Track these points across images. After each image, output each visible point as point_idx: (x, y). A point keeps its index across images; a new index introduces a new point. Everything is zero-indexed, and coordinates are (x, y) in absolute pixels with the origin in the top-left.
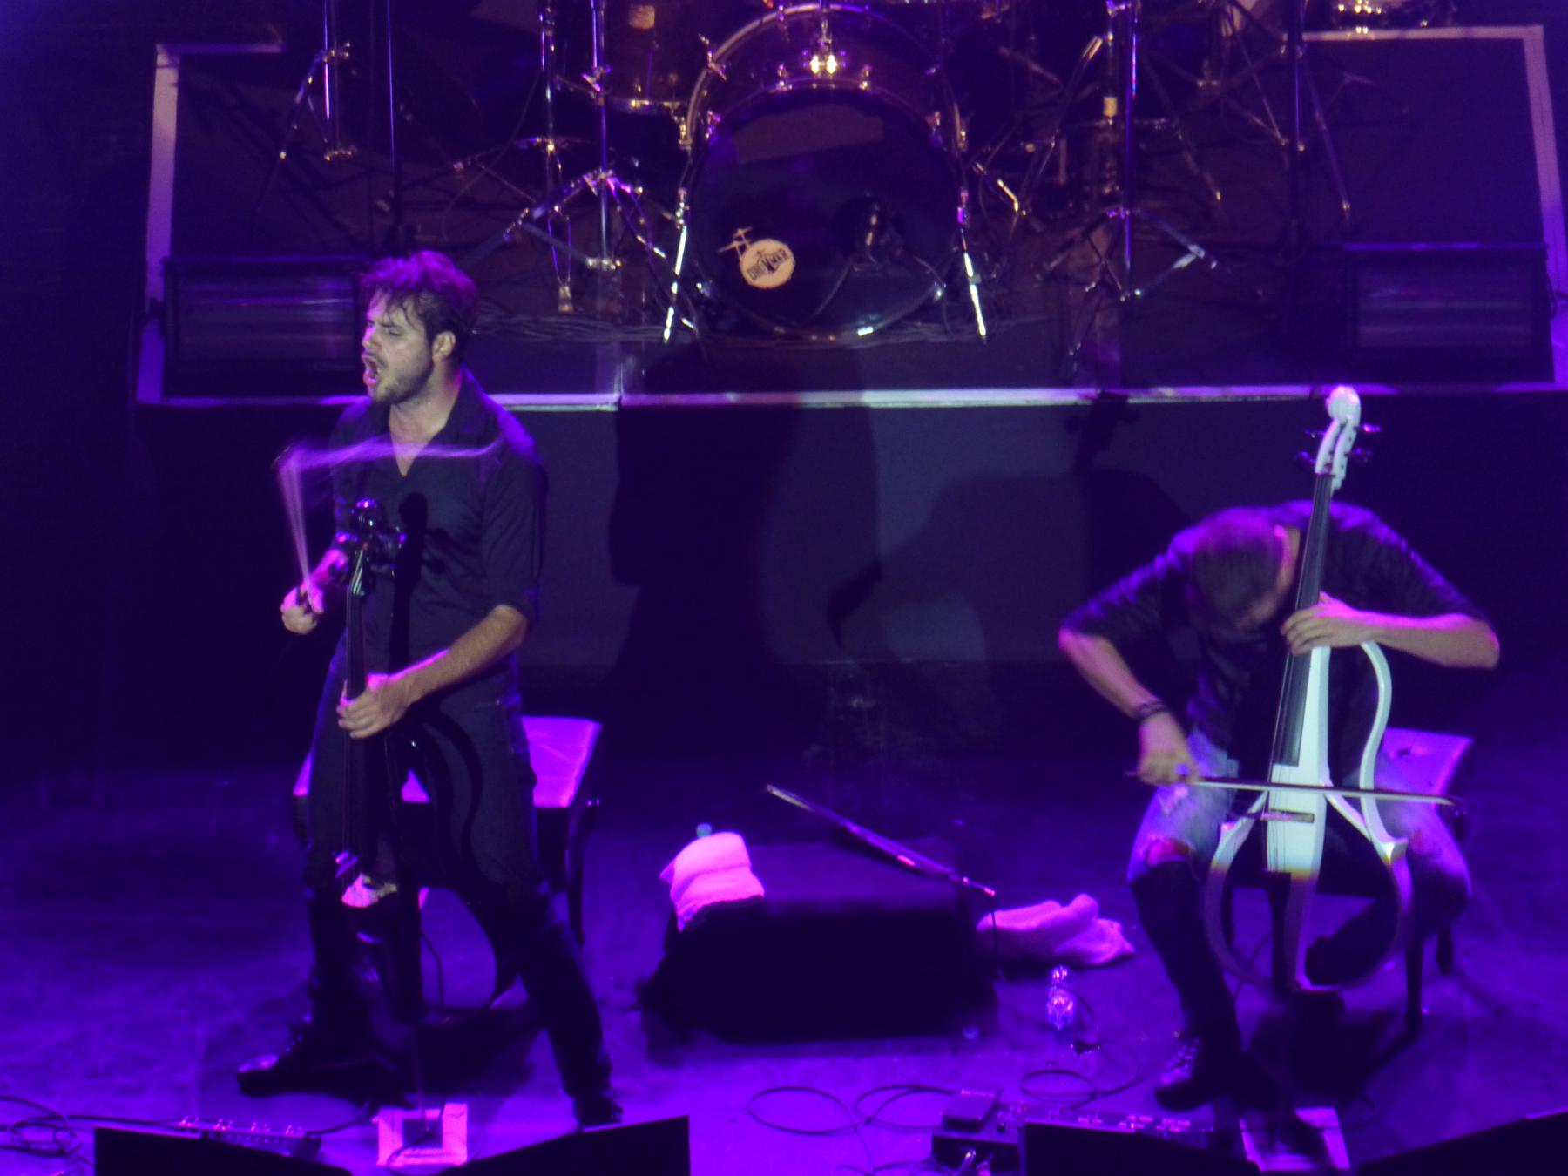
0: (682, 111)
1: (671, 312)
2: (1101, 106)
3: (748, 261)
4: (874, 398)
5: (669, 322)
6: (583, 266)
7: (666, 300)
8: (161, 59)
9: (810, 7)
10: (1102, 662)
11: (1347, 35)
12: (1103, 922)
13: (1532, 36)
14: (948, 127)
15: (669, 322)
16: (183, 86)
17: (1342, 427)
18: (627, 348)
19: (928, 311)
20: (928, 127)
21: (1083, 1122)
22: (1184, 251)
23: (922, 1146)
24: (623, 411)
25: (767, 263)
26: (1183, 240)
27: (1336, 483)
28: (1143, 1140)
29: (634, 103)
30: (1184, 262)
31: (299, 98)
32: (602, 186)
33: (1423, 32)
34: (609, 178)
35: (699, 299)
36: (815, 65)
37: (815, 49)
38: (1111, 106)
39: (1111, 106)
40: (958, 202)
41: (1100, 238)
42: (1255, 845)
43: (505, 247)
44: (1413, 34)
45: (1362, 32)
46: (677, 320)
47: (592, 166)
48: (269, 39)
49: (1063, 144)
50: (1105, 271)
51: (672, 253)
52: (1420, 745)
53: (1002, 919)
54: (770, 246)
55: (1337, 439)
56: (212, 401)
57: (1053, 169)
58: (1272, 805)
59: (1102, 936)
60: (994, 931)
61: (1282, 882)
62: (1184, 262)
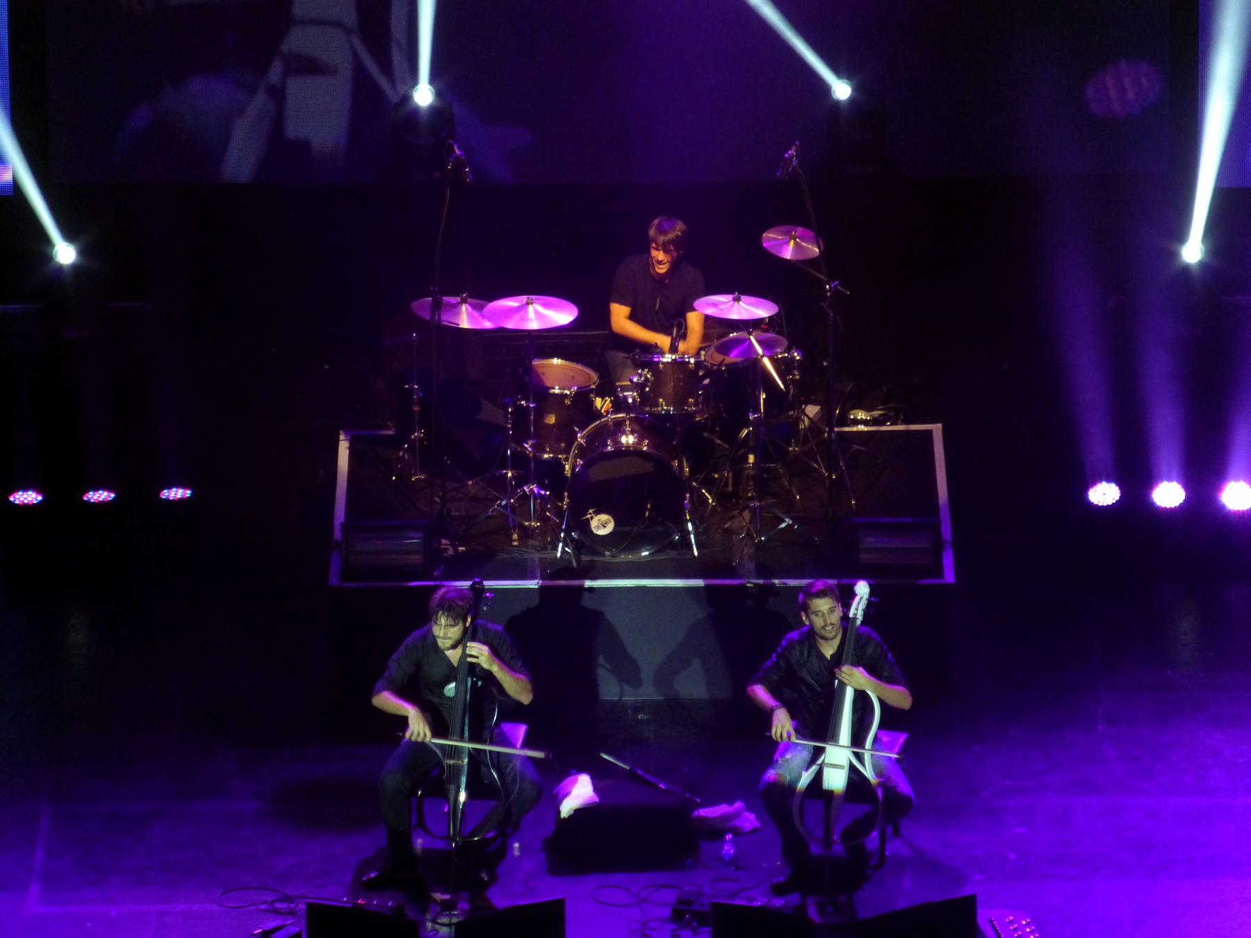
0: (566, 459)
3: (594, 524)
8: (342, 437)
10: (761, 693)
11: (855, 429)
12: (747, 814)
13: (937, 429)
14: (681, 467)
16: (351, 449)
19: (673, 546)
21: (738, 902)
22: (783, 521)
23: (667, 912)
24: (542, 589)
25: (602, 525)
26: (782, 516)
27: (858, 622)
28: (762, 909)
29: (546, 456)
30: (783, 525)
32: (531, 491)
34: (534, 487)
35: (573, 540)
36: (624, 439)
37: (624, 433)
38: (751, 458)
39: (751, 458)
40: (685, 498)
41: (747, 515)
42: (819, 777)
43: (490, 517)
44: (884, 428)
45: (861, 428)
47: (527, 483)
48: (389, 428)
50: (748, 530)
53: (703, 812)
54: (604, 517)
56: (386, 584)
57: (726, 485)
60: (699, 818)
61: (830, 793)
62: (783, 525)
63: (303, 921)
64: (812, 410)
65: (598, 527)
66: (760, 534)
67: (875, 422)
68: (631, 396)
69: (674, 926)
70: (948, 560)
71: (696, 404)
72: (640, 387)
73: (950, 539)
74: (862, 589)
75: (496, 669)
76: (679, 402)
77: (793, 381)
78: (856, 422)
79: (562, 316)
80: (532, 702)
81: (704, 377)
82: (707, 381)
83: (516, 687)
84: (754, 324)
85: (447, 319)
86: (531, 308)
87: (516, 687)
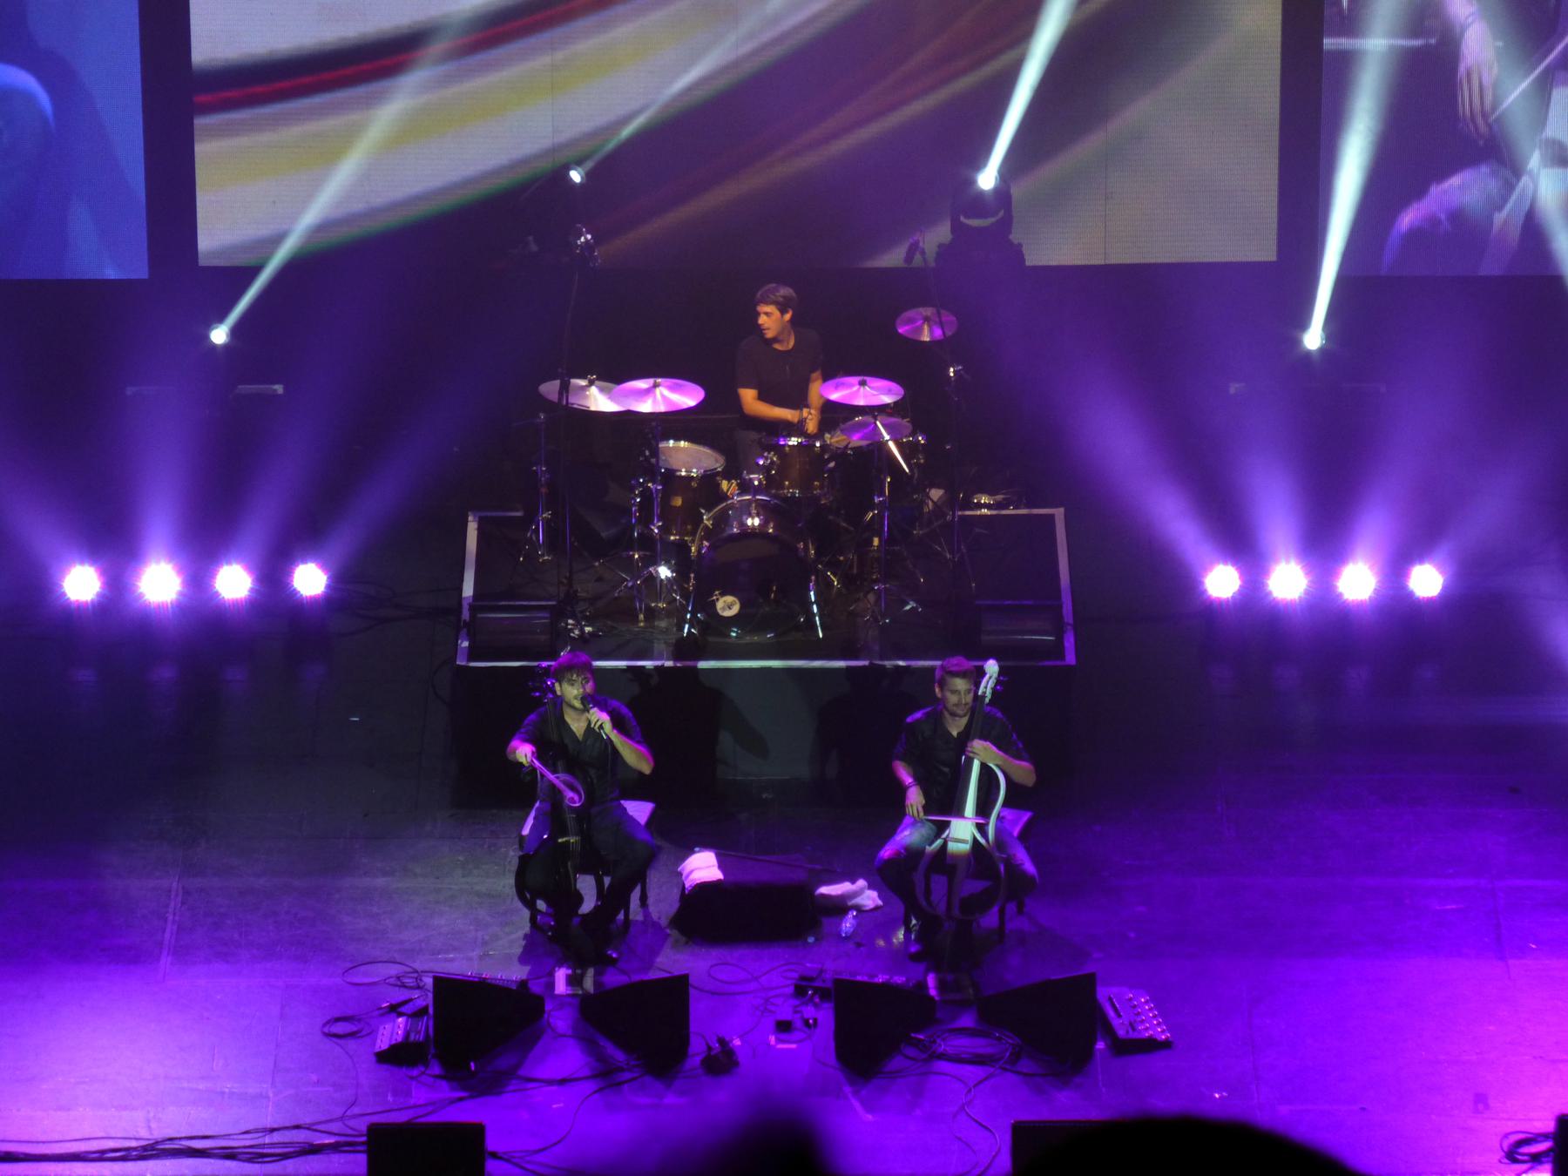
3: (720, 605)
4: (841, 664)
13: (1059, 513)
14: (806, 549)
16: (480, 529)
21: (859, 978)
23: (790, 990)
25: (727, 606)
28: (886, 987)
33: (1011, 511)
35: (699, 621)
38: (876, 541)
39: (876, 541)
41: (871, 597)
44: (1004, 512)
45: (984, 511)
53: (824, 890)
54: (730, 599)
57: (851, 567)
60: (823, 895)
63: (430, 995)
64: (936, 494)
66: (884, 616)
67: (998, 506)
68: (756, 479)
69: (797, 1002)
70: (1069, 642)
71: (821, 487)
72: (766, 470)
74: (992, 667)
75: (615, 738)
76: (805, 485)
77: (917, 464)
78: (980, 506)
79: (686, 398)
81: (829, 461)
82: (832, 465)
83: (634, 757)
84: (882, 409)
85: (576, 401)
86: (658, 391)
87: (634, 757)
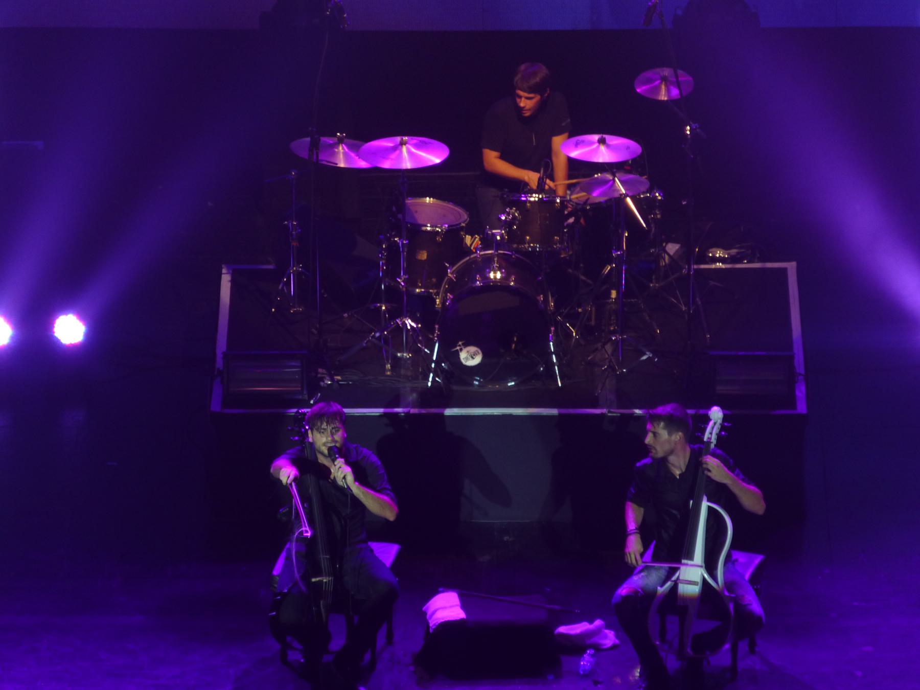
1: (431, 375)
2: (610, 294)
3: (463, 355)
5: (430, 379)
6: (396, 357)
7: (430, 370)
8: (224, 271)
9: (490, 252)
11: (713, 266)
12: (607, 631)
13: (791, 267)
14: (546, 301)
15: (430, 379)
16: (233, 281)
17: (715, 424)
18: (413, 390)
20: (538, 301)
22: (645, 354)
25: (470, 357)
27: (712, 446)
30: (645, 358)
31: (280, 287)
33: (745, 265)
35: (443, 370)
36: (492, 275)
38: (614, 294)
39: (614, 294)
41: (609, 348)
45: (719, 265)
46: (433, 378)
48: (269, 263)
49: (593, 309)
50: (611, 361)
51: (432, 351)
52: (741, 557)
53: (562, 629)
54: (473, 349)
55: (713, 428)
57: (589, 319)
58: (681, 578)
59: (606, 637)
62: (645, 358)
65: (467, 359)
73: (803, 372)
80: (398, 518)
